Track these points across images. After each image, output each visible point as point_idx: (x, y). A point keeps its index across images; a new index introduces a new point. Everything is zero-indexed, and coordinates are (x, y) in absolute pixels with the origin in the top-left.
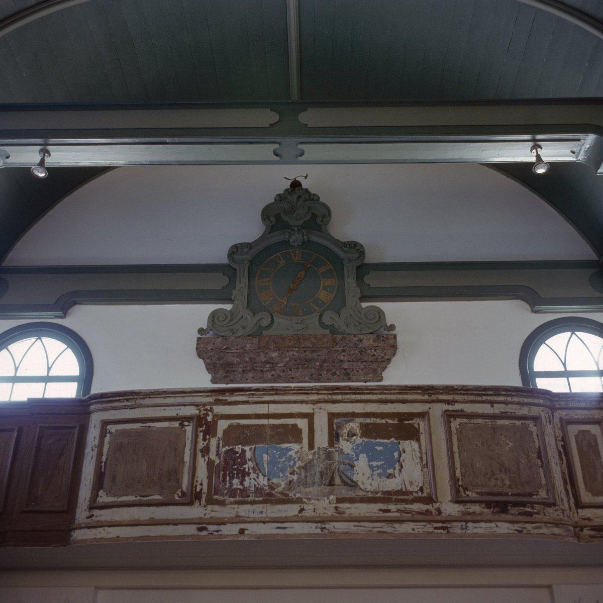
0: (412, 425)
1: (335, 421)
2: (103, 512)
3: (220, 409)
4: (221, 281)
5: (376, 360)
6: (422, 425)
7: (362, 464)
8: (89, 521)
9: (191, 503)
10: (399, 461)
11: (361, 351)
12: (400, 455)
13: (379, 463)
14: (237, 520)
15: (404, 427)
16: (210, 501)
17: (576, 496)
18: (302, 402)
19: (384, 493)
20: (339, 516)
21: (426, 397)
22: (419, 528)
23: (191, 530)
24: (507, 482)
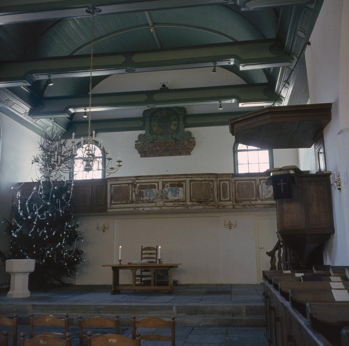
0: (181, 184)
1: (164, 183)
2: (113, 205)
3: (137, 181)
4: (141, 124)
5: (189, 149)
6: (184, 184)
7: (170, 193)
8: (110, 207)
9: (132, 203)
10: (178, 192)
11: (184, 146)
12: (178, 191)
13: (174, 193)
14: (142, 207)
15: (180, 185)
16: (136, 203)
17: (220, 199)
18: (156, 179)
19: (174, 200)
20: (164, 206)
21: (185, 177)
22: (182, 208)
23: (132, 209)
24: (203, 197)
